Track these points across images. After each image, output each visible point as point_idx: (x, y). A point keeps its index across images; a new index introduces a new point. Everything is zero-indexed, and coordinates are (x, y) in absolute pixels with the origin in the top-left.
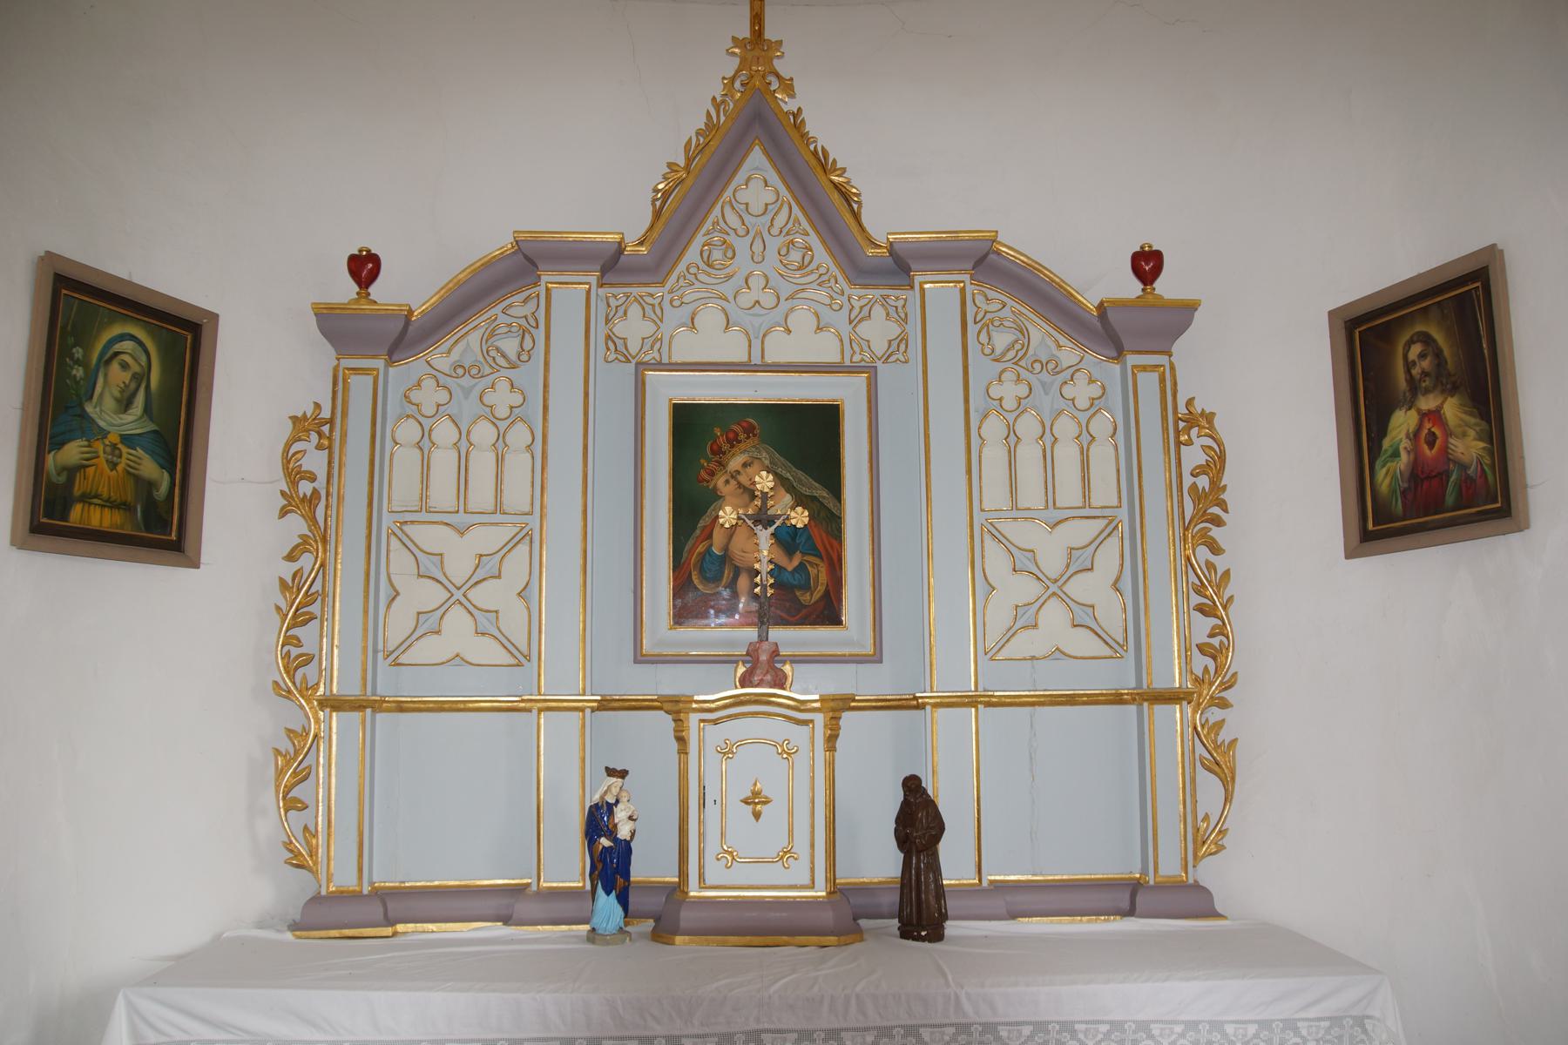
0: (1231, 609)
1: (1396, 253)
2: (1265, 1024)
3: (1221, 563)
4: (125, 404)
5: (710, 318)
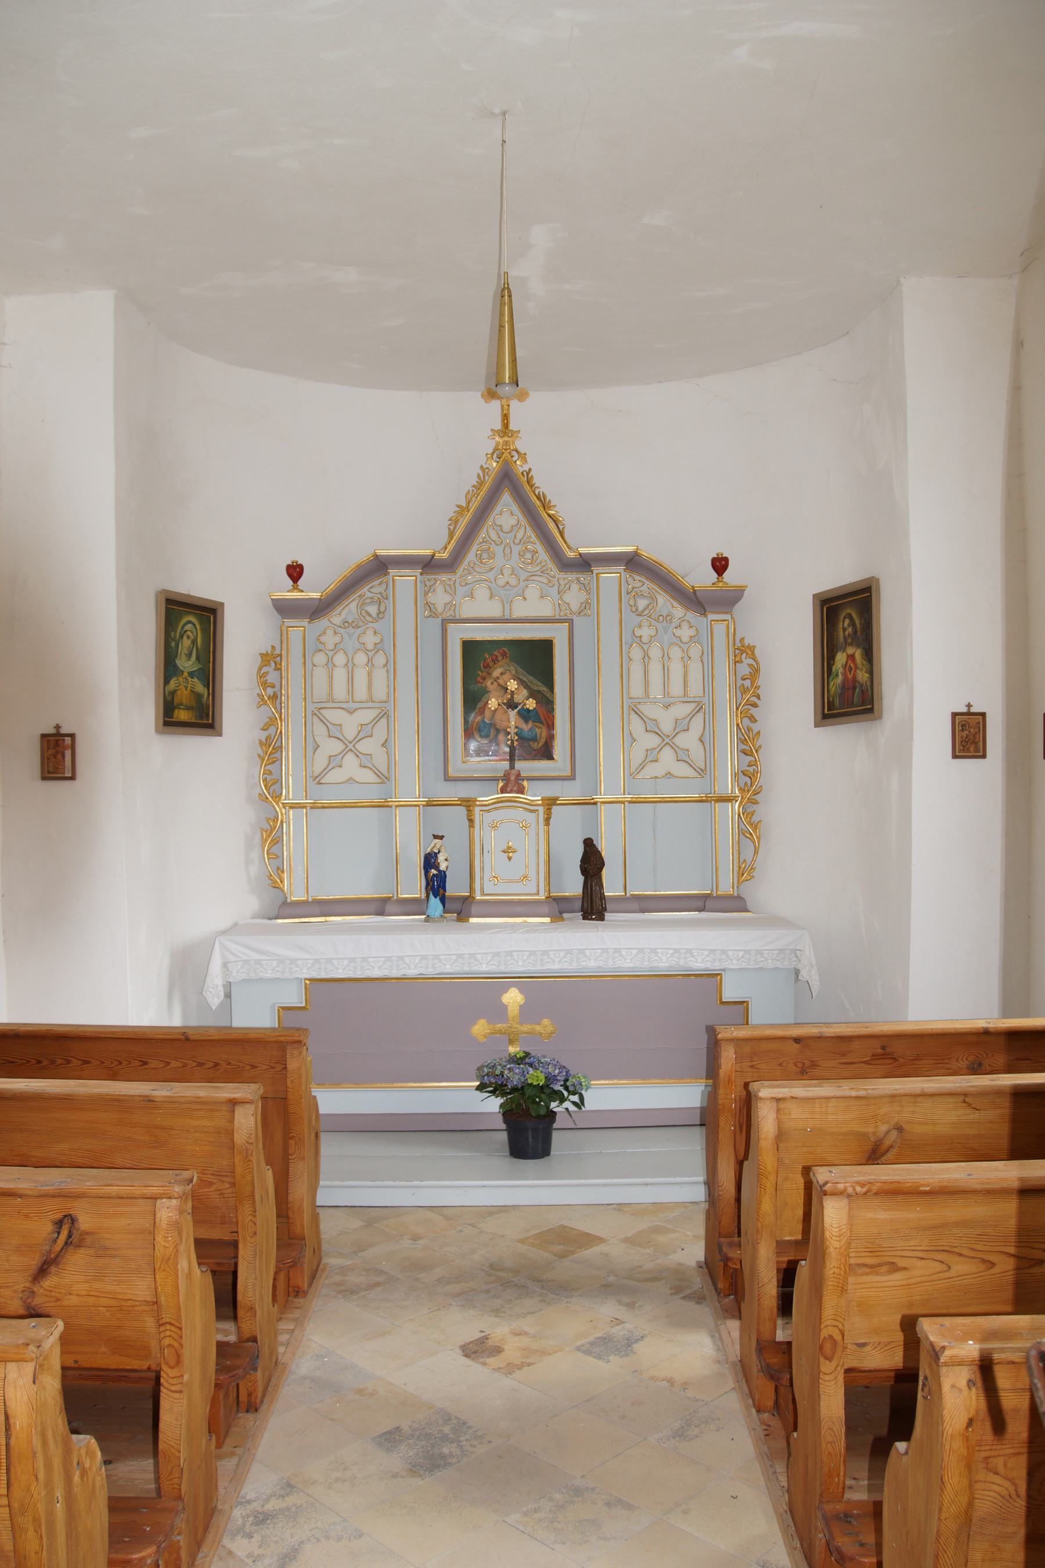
0: (760, 753)
1: (839, 576)
3: (755, 727)
4: (189, 656)
5: (481, 592)
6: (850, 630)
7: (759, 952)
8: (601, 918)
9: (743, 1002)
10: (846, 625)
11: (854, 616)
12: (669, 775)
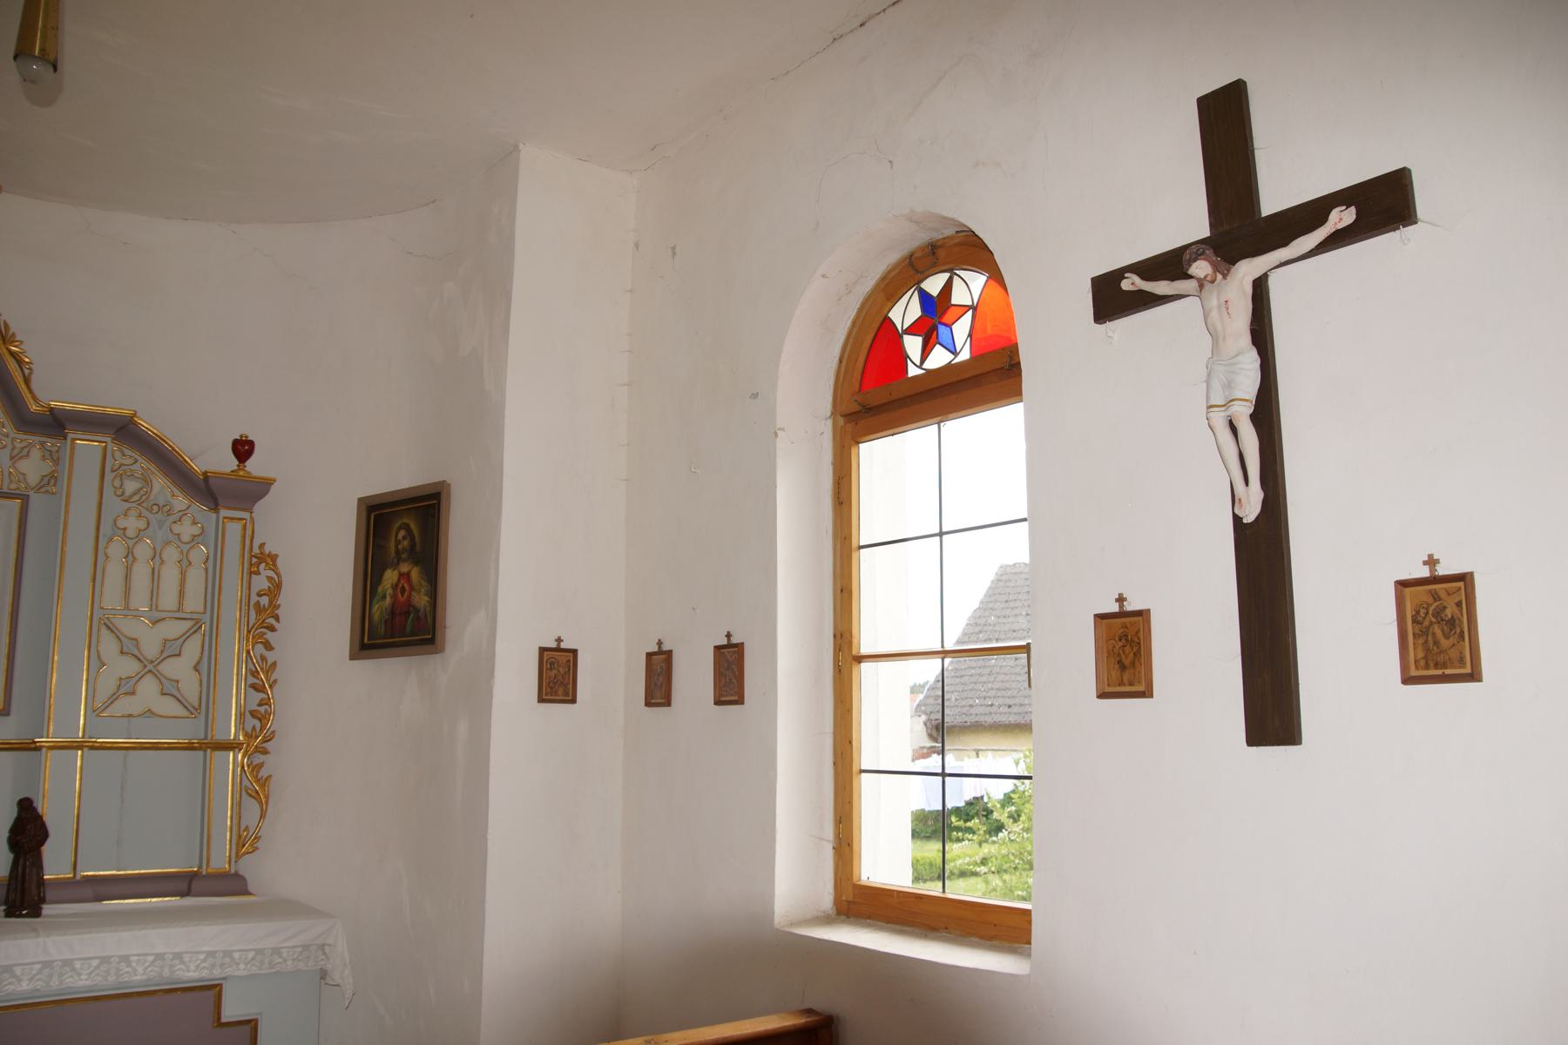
1: (398, 475)
2: (259, 952)
6: (406, 543)
7: (277, 951)
8: (36, 913)
9: (249, 1021)
10: (400, 536)
11: (413, 526)
12: (150, 713)
